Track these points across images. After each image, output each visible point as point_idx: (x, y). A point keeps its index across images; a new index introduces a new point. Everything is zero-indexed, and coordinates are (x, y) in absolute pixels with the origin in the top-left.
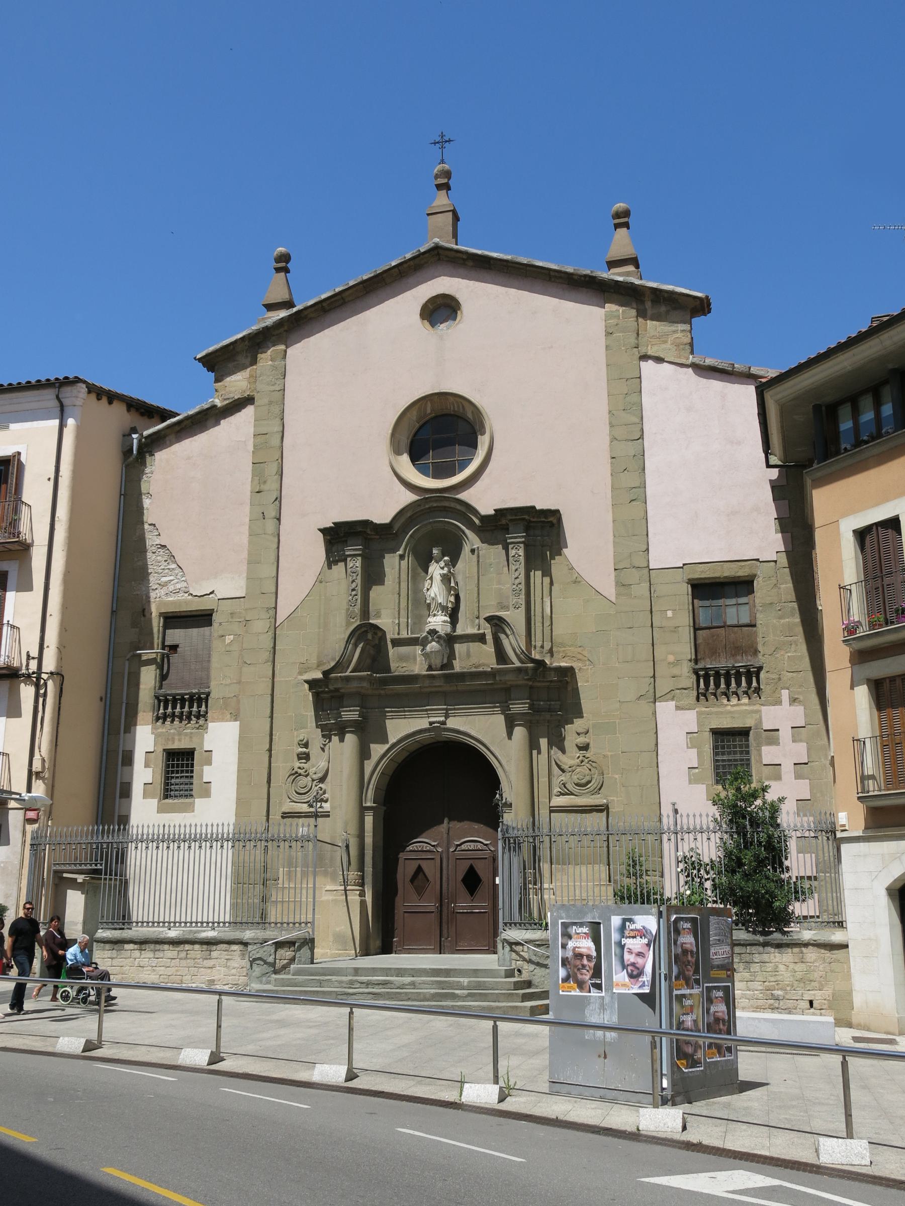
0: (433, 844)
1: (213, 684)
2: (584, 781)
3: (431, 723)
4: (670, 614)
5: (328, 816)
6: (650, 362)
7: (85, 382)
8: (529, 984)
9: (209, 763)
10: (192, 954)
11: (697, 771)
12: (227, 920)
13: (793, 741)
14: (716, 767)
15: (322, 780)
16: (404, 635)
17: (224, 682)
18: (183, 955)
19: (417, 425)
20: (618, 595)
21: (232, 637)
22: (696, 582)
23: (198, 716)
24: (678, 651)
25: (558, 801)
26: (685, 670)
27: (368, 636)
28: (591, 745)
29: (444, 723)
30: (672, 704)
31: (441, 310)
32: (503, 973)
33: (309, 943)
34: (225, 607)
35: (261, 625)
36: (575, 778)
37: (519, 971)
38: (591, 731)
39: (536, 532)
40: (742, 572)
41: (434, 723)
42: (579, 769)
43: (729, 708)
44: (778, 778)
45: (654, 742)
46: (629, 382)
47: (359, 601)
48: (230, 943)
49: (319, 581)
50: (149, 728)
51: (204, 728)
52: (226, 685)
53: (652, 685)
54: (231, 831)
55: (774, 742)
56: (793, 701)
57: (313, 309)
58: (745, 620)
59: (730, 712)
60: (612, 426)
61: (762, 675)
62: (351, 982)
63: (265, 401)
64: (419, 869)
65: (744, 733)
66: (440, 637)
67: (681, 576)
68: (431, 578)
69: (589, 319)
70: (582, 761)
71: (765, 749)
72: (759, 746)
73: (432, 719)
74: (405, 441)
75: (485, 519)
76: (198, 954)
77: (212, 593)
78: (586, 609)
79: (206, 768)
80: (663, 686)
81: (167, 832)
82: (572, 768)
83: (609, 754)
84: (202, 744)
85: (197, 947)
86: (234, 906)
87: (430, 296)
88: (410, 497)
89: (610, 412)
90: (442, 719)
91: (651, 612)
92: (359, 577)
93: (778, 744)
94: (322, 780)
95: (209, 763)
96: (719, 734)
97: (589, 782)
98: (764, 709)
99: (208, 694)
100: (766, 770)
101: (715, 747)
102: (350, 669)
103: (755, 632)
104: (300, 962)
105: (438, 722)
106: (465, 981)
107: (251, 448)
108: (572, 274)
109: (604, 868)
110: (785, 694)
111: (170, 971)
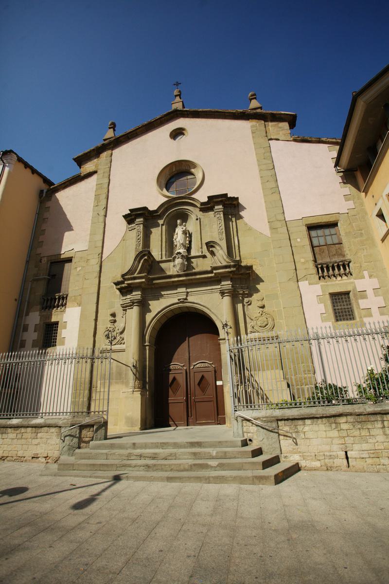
0: (182, 365)
1: (70, 290)
2: (264, 325)
3: (179, 300)
4: (299, 240)
5: (125, 351)
6: (273, 141)
7: (16, 154)
8: (275, 460)
9: (65, 328)
10: (25, 435)
11: (325, 315)
12: (69, 411)
13: (375, 296)
14: (335, 313)
15: (122, 333)
16: (164, 258)
17: (75, 289)
18: (20, 436)
19: (169, 177)
20: (272, 233)
21: (80, 268)
22: (309, 226)
23: (62, 305)
24: (305, 257)
25: (251, 336)
26: (311, 265)
27: (144, 254)
28: (266, 306)
29: (186, 299)
30: (307, 282)
31: (177, 133)
32: (240, 444)
33: (105, 424)
34: (78, 255)
35: (95, 261)
36: (259, 323)
37: (250, 440)
38: (265, 298)
39: (229, 206)
40: (332, 219)
41: (180, 299)
42: (260, 319)
43: (337, 282)
44: (371, 315)
45: (300, 302)
46: (265, 149)
47: (141, 244)
48: (49, 426)
49: (123, 239)
50: (38, 313)
51: (64, 311)
52: (76, 290)
53: (295, 273)
54: (74, 352)
55: (365, 297)
56: (370, 276)
57: (124, 137)
58: (336, 241)
59: (338, 284)
60: (259, 165)
61: (350, 264)
62: (130, 455)
63: (102, 172)
64: (203, 377)
65: (347, 293)
66: (182, 256)
67: (300, 223)
68: (177, 234)
69: (244, 127)
70: (262, 314)
71: (360, 301)
72: (357, 299)
73: (179, 298)
74: (164, 182)
75: (202, 204)
76: (29, 435)
77: (73, 249)
78: (257, 239)
79: (63, 330)
80: (301, 274)
81: (79, 376)
82: (257, 319)
83: (276, 309)
84: (62, 319)
85: (29, 429)
86: (73, 403)
87: (173, 129)
88: (166, 199)
89: (258, 160)
90: (185, 297)
91: (290, 240)
92: (142, 233)
93: (367, 298)
94: (122, 333)
95: (65, 328)
96: (333, 295)
97: (267, 325)
98: (356, 281)
99: (67, 296)
100: (363, 312)
101: (333, 303)
102: (136, 273)
103: (343, 247)
104: (96, 439)
105: (183, 299)
106: (214, 452)
107: (95, 189)
108: (235, 113)
109: (279, 373)
110: (366, 273)
111: (10, 448)
